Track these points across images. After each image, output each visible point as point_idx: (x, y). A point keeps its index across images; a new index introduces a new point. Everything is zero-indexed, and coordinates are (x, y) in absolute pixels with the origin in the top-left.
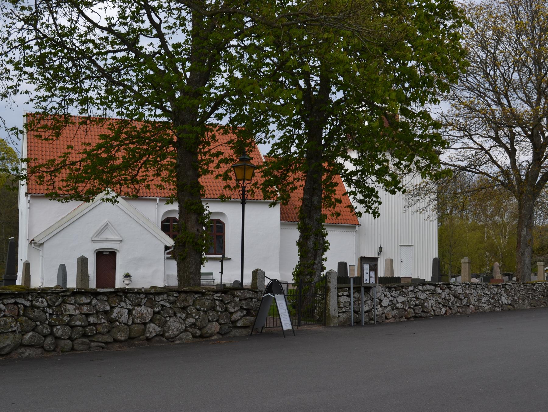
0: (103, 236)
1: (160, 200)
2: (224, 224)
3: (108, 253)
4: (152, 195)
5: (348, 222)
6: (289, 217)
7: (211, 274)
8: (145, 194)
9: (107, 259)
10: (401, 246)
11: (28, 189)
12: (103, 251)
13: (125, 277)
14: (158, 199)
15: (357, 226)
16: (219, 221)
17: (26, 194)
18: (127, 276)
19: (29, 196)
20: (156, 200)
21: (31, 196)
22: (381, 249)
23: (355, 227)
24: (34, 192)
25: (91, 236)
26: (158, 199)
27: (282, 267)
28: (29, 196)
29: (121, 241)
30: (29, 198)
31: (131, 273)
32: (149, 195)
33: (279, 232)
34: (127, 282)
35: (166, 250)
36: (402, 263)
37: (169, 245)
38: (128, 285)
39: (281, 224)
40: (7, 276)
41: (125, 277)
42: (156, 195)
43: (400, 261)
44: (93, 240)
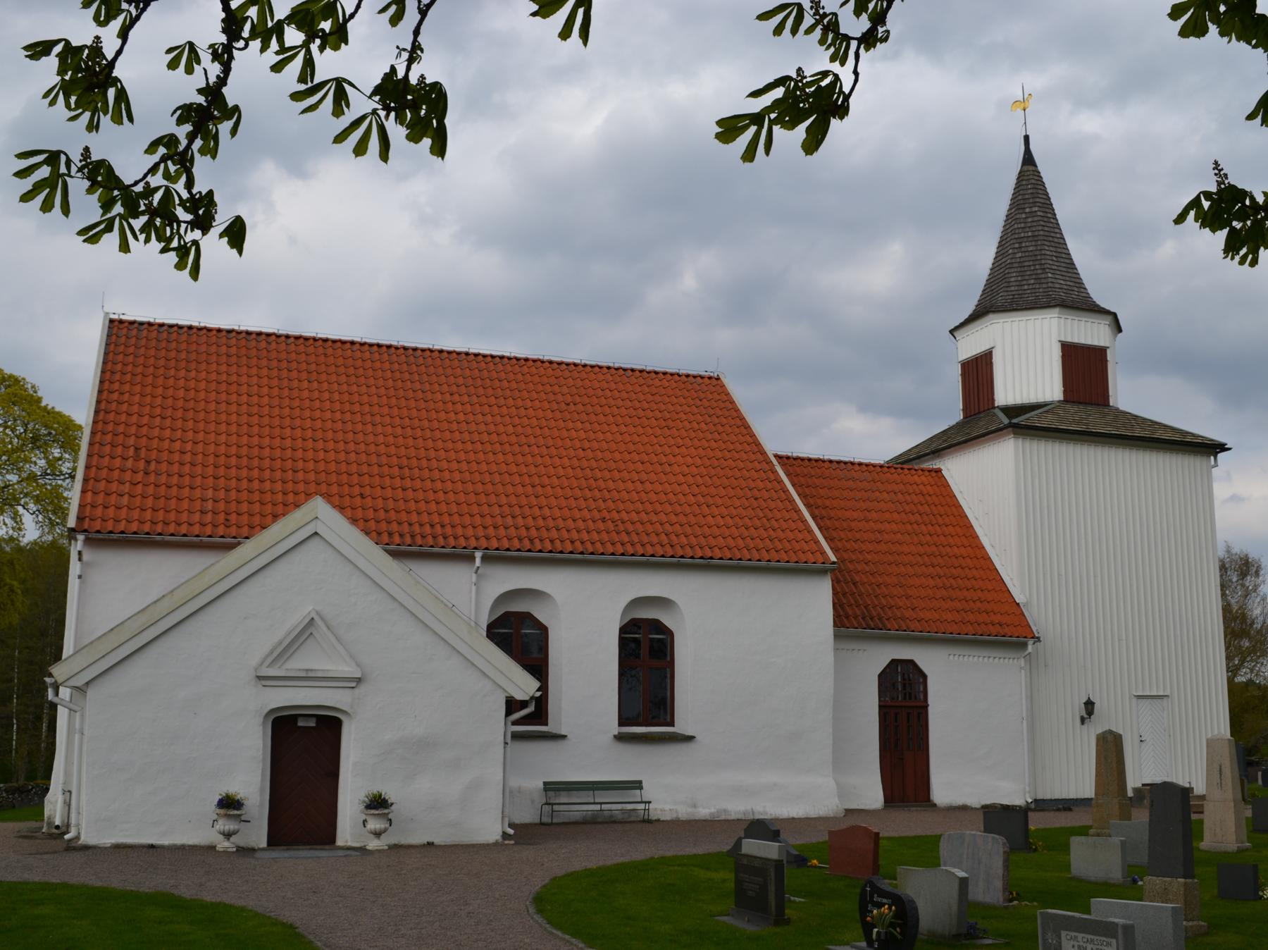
0: (298, 663)
1: (484, 558)
2: (544, 630)
3: (312, 723)
4: (462, 542)
5: (1007, 630)
6: (847, 617)
7: (638, 785)
8: (441, 541)
9: (304, 748)
10: (1139, 697)
12: (296, 717)
13: (368, 807)
14: (478, 555)
15: (1031, 642)
16: (657, 626)
18: (377, 803)
19: (81, 537)
20: (471, 559)
21: (88, 541)
22: (1089, 706)
23: (1024, 645)
24: (97, 525)
25: (255, 662)
26: (478, 555)
27: (840, 761)
28: (81, 537)
31: (390, 793)
32: (452, 542)
33: (830, 658)
34: (374, 824)
35: (509, 712)
36: (1144, 745)
37: (520, 696)
38: (378, 834)
39: (837, 636)
41: (368, 807)
42: (473, 543)
43: (1137, 739)
44: (260, 678)
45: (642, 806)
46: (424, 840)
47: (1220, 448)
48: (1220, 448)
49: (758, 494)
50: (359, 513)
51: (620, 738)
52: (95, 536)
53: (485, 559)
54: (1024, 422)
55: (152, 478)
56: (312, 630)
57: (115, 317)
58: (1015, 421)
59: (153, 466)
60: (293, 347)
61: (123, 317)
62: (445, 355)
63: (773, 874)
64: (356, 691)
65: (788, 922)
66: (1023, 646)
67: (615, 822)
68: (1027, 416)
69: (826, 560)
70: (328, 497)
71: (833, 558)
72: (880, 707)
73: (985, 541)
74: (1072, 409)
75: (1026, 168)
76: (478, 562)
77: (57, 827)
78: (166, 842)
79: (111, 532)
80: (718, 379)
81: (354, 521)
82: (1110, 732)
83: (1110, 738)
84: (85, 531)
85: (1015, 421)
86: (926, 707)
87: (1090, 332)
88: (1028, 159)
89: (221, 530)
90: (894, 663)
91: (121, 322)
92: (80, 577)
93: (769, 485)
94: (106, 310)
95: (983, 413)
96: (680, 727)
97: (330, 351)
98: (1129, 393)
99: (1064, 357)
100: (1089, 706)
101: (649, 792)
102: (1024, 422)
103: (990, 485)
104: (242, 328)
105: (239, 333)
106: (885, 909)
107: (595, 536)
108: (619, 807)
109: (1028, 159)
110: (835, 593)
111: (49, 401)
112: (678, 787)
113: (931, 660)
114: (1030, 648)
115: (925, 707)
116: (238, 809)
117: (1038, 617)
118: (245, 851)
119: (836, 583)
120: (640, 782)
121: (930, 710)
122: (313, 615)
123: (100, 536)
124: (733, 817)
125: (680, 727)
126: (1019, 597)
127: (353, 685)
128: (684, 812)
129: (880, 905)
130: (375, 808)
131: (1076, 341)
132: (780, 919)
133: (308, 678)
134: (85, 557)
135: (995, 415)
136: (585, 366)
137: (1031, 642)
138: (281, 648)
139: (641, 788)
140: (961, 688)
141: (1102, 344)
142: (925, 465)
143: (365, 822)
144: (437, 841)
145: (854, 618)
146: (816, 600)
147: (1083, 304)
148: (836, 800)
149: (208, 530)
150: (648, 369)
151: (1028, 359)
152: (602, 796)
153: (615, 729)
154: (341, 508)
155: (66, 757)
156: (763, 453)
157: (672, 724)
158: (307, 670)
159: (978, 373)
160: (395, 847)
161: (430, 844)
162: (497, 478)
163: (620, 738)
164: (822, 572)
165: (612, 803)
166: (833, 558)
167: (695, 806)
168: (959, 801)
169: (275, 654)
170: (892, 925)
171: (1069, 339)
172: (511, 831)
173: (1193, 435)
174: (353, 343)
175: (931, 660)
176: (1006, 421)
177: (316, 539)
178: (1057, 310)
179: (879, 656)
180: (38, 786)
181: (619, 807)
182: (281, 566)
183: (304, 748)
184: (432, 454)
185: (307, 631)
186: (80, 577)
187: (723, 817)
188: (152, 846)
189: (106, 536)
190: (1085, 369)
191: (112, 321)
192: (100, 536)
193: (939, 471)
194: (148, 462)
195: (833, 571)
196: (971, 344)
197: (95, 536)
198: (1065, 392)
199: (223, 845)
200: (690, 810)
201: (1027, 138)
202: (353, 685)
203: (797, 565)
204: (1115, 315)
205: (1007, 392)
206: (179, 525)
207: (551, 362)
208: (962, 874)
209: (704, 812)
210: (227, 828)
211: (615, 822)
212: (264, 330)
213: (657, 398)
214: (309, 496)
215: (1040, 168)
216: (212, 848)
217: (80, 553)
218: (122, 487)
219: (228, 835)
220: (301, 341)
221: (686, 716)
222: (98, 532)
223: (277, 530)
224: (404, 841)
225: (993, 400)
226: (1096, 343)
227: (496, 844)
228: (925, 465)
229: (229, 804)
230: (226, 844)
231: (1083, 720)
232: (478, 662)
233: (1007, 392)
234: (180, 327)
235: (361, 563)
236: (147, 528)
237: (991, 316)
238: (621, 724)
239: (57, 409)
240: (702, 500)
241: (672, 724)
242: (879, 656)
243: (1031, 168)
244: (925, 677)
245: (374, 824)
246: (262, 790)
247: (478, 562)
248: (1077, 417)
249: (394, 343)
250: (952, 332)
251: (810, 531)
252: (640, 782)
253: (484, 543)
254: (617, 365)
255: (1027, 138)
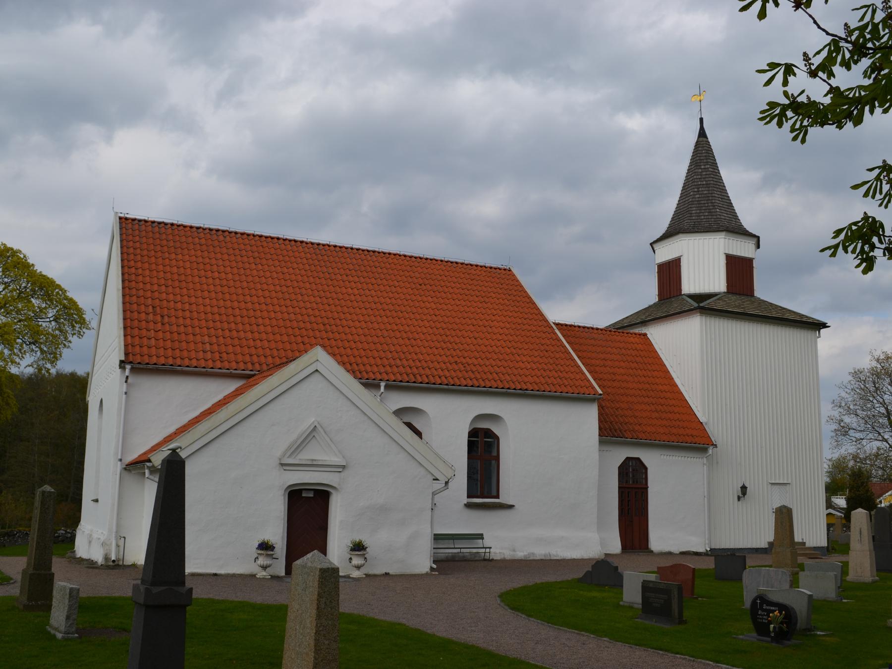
0: (305, 456)
1: (386, 387)
3: (311, 495)
7: (480, 536)
8: (250, 366)
9: (308, 510)
11: (126, 354)
12: (301, 490)
14: (383, 384)
17: (122, 362)
19: (128, 367)
20: (379, 387)
21: (133, 370)
22: (744, 489)
24: (138, 359)
25: (279, 453)
26: (383, 384)
28: (128, 367)
29: (344, 467)
30: (127, 372)
31: (366, 543)
38: (358, 567)
39: (601, 442)
40: (156, 590)
41: (353, 549)
42: (379, 377)
44: (282, 465)
45: (483, 550)
46: (383, 572)
47: (824, 325)
48: (824, 325)
49: (547, 348)
50: (346, 359)
51: (468, 506)
52: (138, 366)
53: (387, 387)
54: (703, 304)
55: (167, 327)
56: (314, 434)
57: (122, 215)
58: (701, 305)
59: (166, 319)
60: (157, 229)
61: (128, 216)
62: (220, 233)
63: (676, 593)
64: (342, 474)
65: (685, 622)
66: (705, 450)
67: (465, 560)
68: (708, 301)
69: (596, 393)
70: (324, 347)
71: (600, 392)
72: (619, 488)
73: (678, 382)
74: (734, 298)
75: (701, 139)
76: (382, 388)
77: (114, 561)
78: (222, 572)
79: (148, 364)
80: (510, 270)
81: (342, 363)
82: (784, 507)
83: (784, 511)
84: (131, 362)
85: (701, 305)
86: (646, 488)
87: (742, 248)
88: (702, 134)
89: (218, 364)
90: (628, 459)
91: (126, 219)
92: (126, 393)
93: (554, 343)
94: (116, 210)
95: (672, 298)
96: (503, 499)
97: (265, 244)
98: (766, 289)
99: (727, 264)
100: (744, 489)
101: (487, 542)
102: (703, 304)
103: (679, 345)
104: (206, 226)
105: (204, 229)
106: (776, 613)
107: (453, 374)
108: (468, 550)
109: (702, 134)
110: (600, 414)
111: (39, 268)
112: (505, 538)
113: (651, 459)
114: (710, 451)
115: (645, 489)
116: (272, 550)
117: (715, 431)
118: (274, 578)
119: (601, 409)
120: (482, 535)
121: (649, 490)
122: (316, 424)
123: (141, 366)
124: (538, 558)
125: (503, 499)
126: (702, 419)
127: (340, 470)
128: (508, 554)
129: (773, 612)
130: (358, 550)
131: (739, 254)
132: (681, 621)
133: (313, 465)
134: (129, 381)
135: (684, 300)
136: (427, 259)
137: (711, 447)
138: (295, 446)
139: (483, 539)
140: (669, 477)
141: (750, 256)
142: (637, 331)
143: (351, 559)
144: (391, 572)
145: (611, 431)
146: (587, 418)
147: (737, 230)
148: (599, 548)
149: (210, 364)
150: (466, 262)
151: (703, 264)
152: (459, 544)
153: (465, 500)
154: (333, 355)
155: (118, 515)
156: (546, 321)
157: (497, 497)
158: (313, 460)
159: (669, 273)
160: (367, 575)
161: (387, 574)
162: (386, 334)
163: (468, 506)
164: (592, 400)
165: (466, 549)
166: (600, 392)
167: (514, 551)
168: (666, 549)
169: (293, 449)
170: (782, 623)
171: (731, 253)
172: (435, 566)
173: (807, 317)
174: (278, 239)
175: (651, 459)
176: (696, 305)
177: (317, 374)
178: (724, 233)
179: (620, 455)
180: (20, 531)
181: (468, 550)
182: (295, 391)
183: (308, 510)
184: (257, 306)
185: (312, 434)
186: (126, 393)
187: (531, 558)
188: (215, 575)
189: (145, 366)
190: (739, 271)
191: (120, 218)
192: (141, 366)
193: (645, 335)
194: (162, 316)
195: (598, 399)
196: (666, 252)
197: (138, 366)
198: (728, 287)
199: (261, 574)
200: (512, 553)
201: (701, 120)
202: (340, 470)
203: (576, 395)
204: (758, 238)
205: (691, 284)
206: (191, 360)
207: (236, 233)
208: (809, 593)
209: (520, 555)
210: (265, 563)
211: (465, 560)
212: (220, 228)
213: (474, 282)
214: (312, 346)
215: (710, 140)
216: (253, 576)
217: (127, 377)
218: (149, 333)
219: (264, 568)
220: (162, 225)
221: (508, 490)
222: (139, 363)
223: (292, 367)
224: (370, 573)
225: (681, 290)
226: (747, 255)
227: (427, 574)
228: (637, 331)
229: (265, 547)
230: (264, 573)
231: (739, 498)
232: (418, 456)
233: (691, 284)
234: (166, 224)
235: (345, 390)
236: (171, 361)
237: (681, 235)
238: (469, 497)
239: (44, 273)
240: (514, 351)
241: (497, 497)
242: (620, 455)
243: (705, 139)
244: (646, 469)
245: (356, 561)
246: (283, 537)
247: (382, 388)
248: (736, 303)
249: (175, 222)
250: (651, 244)
251: (583, 374)
252: (482, 535)
253: (386, 377)
254: (446, 259)
255: (701, 120)
